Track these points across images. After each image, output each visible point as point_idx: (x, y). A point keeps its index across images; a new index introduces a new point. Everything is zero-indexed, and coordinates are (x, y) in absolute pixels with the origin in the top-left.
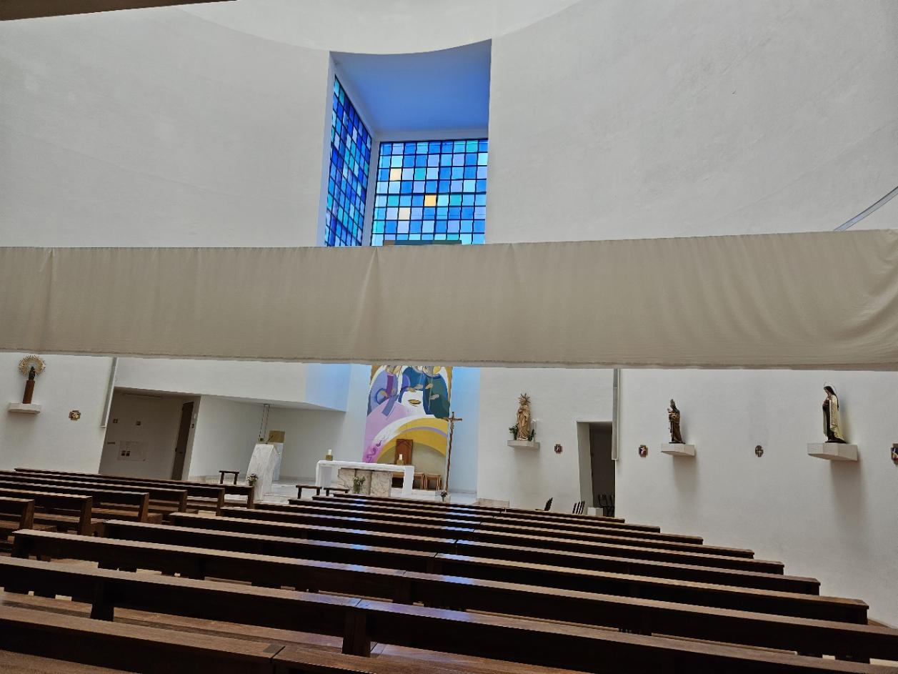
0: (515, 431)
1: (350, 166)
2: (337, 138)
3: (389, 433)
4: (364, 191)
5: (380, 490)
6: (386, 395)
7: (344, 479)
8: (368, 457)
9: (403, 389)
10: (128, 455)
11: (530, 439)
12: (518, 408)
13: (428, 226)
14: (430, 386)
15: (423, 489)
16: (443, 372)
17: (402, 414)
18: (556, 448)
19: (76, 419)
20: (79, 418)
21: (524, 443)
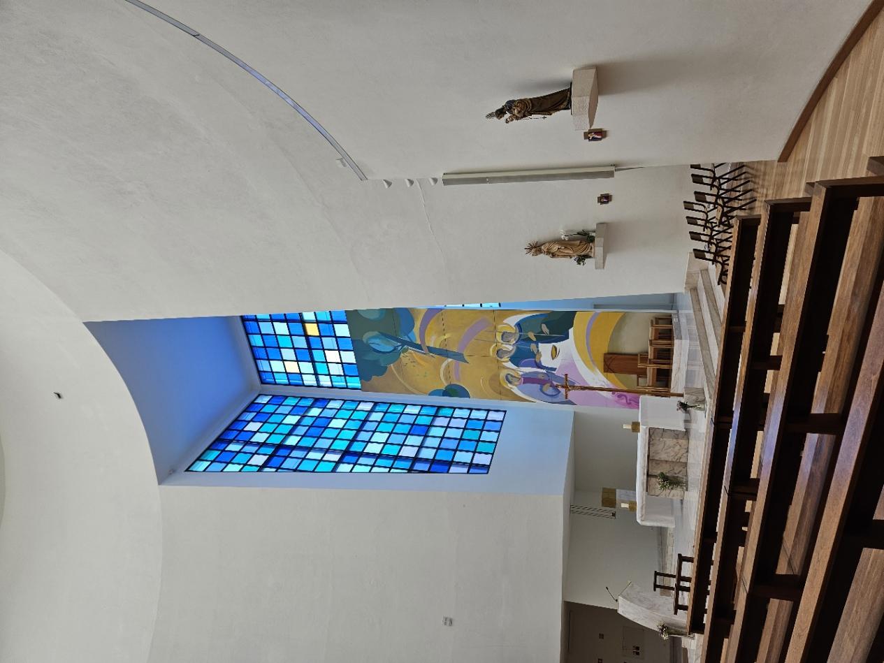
0: (581, 259)
1: (286, 432)
8: (630, 403)
9: (539, 366)
10: (638, 648)
11: (592, 240)
15: (672, 345)
16: (513, 321)
17: (572, 365)
21: (598, 250)
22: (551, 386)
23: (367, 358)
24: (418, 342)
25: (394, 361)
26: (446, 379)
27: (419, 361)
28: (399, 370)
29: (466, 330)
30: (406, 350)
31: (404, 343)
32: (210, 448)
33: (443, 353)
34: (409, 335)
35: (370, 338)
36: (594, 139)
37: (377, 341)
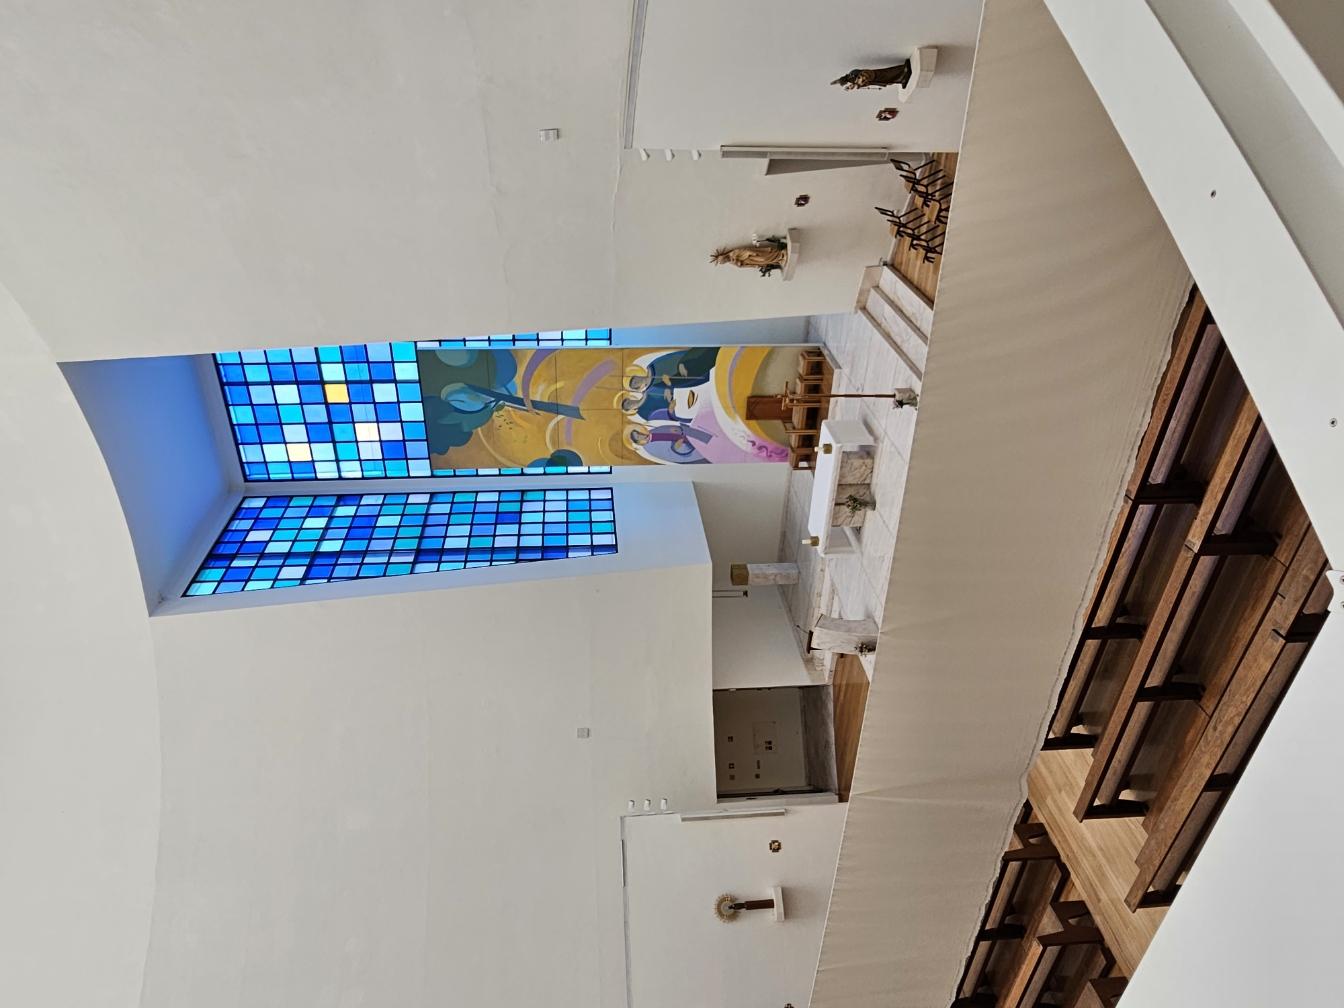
0: (767, 269)
2: (286, 573)
3: (738, 431)
4: (342, 499)
5: (862, 470)
6: (680, 440)
7: (842, 519)
8: (770, 456)
9: (672, 417)
10: (770, 743)
12: (736, 267)
13: (384, 393)
14: (666, 379)
16: (645, 361)
17: (710, 415)
18: (799, 205)
19: (779, 845)
20: (777, 841)
22: (684, 442)
23: (444, 423)
24: (520, 394)
25: (484, 424)
26: (553, 443)
27: (519, 421)
28: (489, 435)
29: (585, 376)
30: (502, 407)
31: (499, 397)
32: (204, 567)
33: (553, 408)
34: (508, 386)
35: (451, 394)
36: (886, 119)
37: (462, 397)
